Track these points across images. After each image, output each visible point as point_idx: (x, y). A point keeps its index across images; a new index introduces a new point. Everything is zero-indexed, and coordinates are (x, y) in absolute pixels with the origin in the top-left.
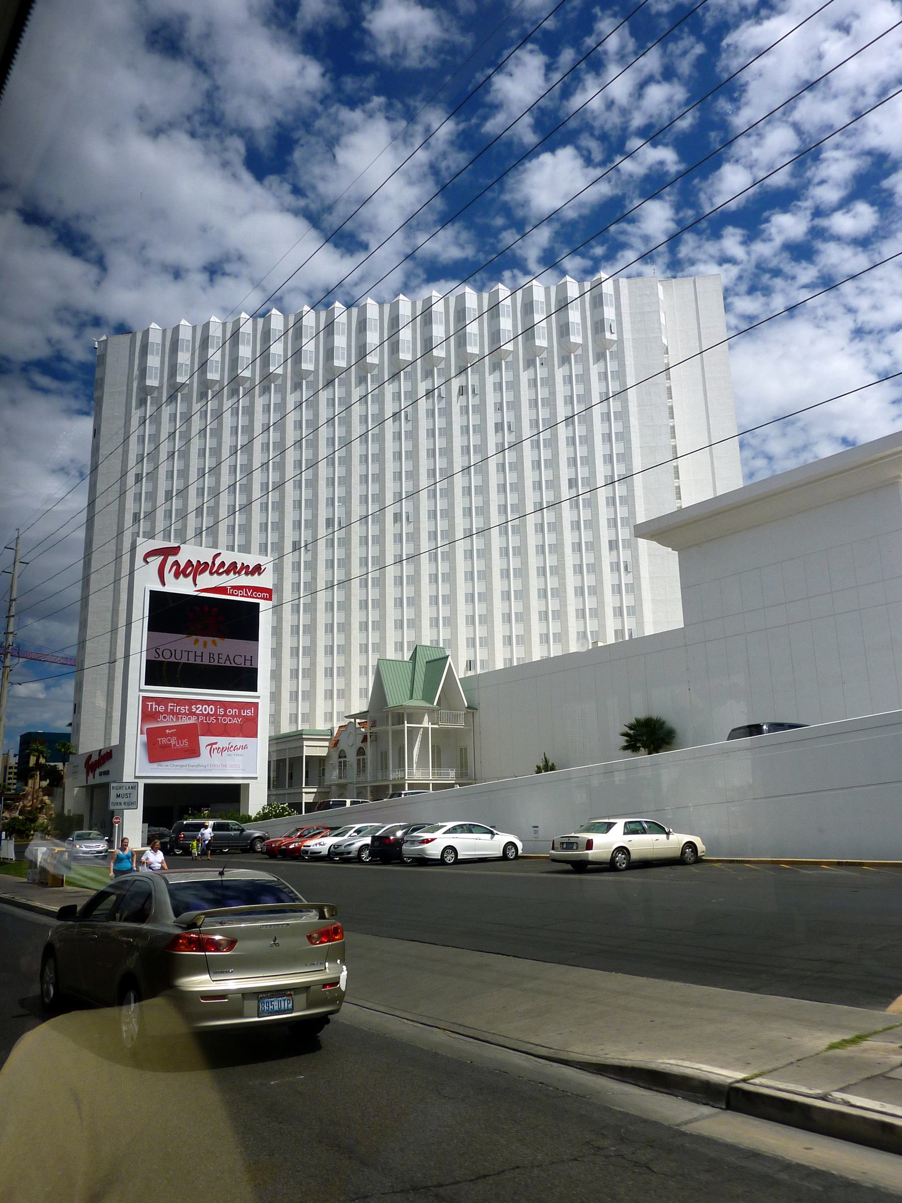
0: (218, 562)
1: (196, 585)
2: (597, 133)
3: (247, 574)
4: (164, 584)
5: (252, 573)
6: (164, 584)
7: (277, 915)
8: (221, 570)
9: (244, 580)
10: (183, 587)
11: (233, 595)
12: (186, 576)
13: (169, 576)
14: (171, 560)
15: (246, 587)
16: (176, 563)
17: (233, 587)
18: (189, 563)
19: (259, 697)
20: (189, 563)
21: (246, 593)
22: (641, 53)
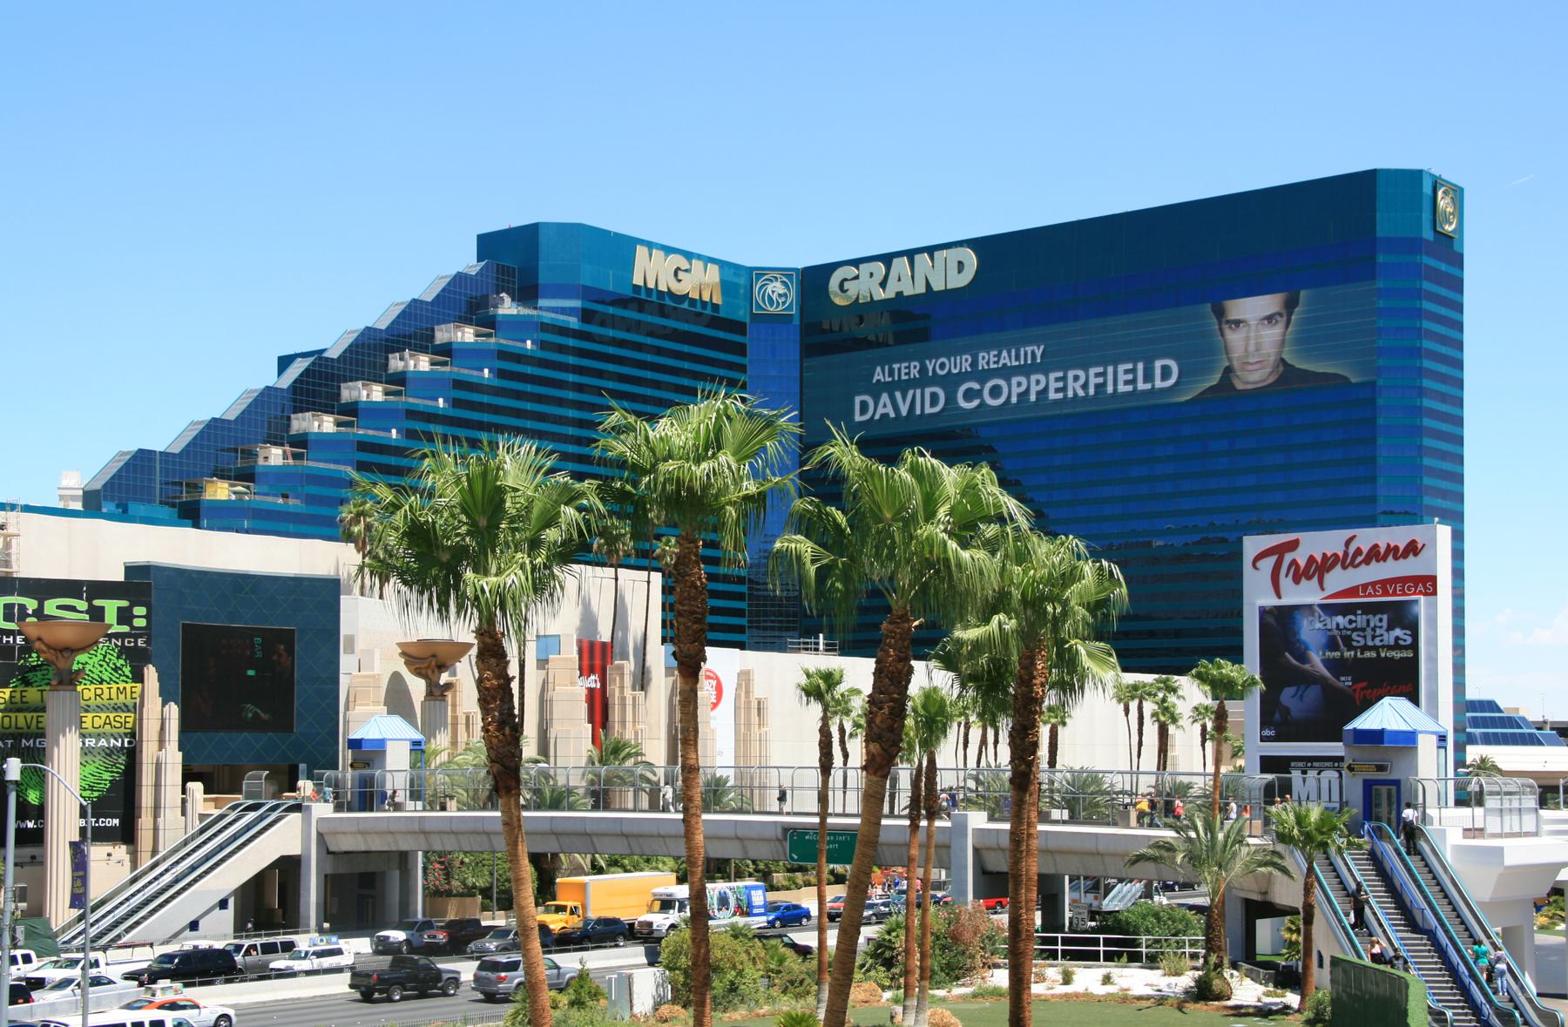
0: (1352, 550)
2: (593, 681)
3: (1396, 558)
4: (1279, 597)
5: (1405, 555)
6: (1279, 597)
8: (1360, 559)
12: (1309, 578)
13: (1286, 582)
14: (1288, 557)
16: (1294, 562)
18: (1311, 559)
20: (1311, 559)
22: (632, 561)
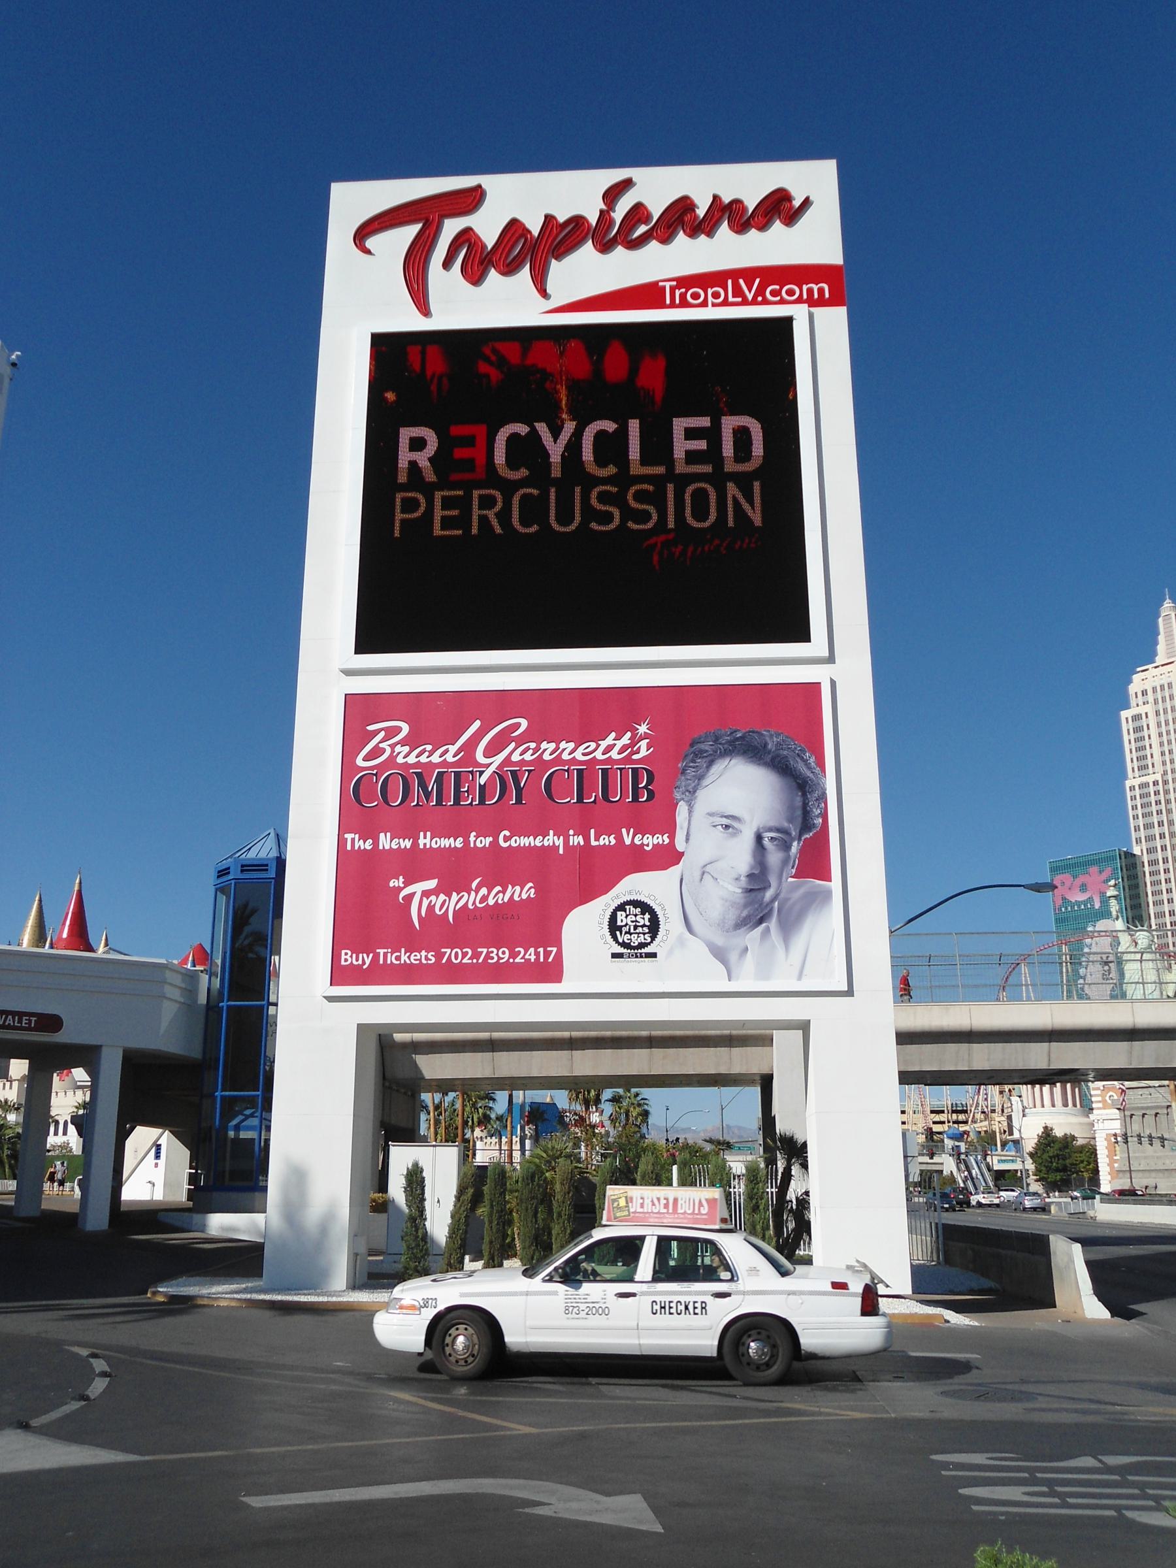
1: (544, 293)
4: (424, 308)
6: (424, 308)
7: (608, 1034)
9: (726, 250)
10: (506, 304)
11: (684, 304)
12: (509, 269)
13: (445, 282)
14: (451, 228)
15: (735, 274)
17: (685, 282)
18: (514, 228)
19: (349, 673)
20: (514, 228)
21: (738, 292)
